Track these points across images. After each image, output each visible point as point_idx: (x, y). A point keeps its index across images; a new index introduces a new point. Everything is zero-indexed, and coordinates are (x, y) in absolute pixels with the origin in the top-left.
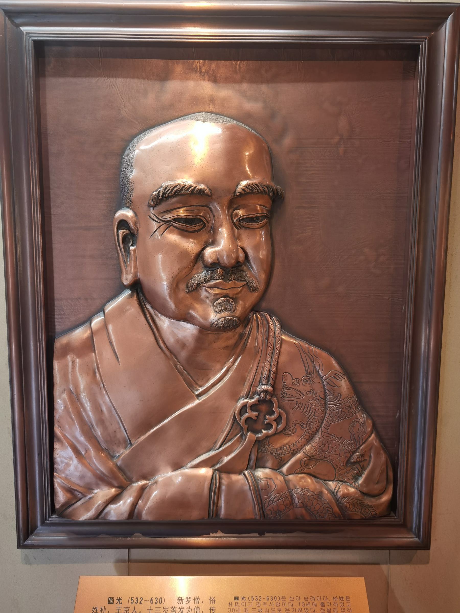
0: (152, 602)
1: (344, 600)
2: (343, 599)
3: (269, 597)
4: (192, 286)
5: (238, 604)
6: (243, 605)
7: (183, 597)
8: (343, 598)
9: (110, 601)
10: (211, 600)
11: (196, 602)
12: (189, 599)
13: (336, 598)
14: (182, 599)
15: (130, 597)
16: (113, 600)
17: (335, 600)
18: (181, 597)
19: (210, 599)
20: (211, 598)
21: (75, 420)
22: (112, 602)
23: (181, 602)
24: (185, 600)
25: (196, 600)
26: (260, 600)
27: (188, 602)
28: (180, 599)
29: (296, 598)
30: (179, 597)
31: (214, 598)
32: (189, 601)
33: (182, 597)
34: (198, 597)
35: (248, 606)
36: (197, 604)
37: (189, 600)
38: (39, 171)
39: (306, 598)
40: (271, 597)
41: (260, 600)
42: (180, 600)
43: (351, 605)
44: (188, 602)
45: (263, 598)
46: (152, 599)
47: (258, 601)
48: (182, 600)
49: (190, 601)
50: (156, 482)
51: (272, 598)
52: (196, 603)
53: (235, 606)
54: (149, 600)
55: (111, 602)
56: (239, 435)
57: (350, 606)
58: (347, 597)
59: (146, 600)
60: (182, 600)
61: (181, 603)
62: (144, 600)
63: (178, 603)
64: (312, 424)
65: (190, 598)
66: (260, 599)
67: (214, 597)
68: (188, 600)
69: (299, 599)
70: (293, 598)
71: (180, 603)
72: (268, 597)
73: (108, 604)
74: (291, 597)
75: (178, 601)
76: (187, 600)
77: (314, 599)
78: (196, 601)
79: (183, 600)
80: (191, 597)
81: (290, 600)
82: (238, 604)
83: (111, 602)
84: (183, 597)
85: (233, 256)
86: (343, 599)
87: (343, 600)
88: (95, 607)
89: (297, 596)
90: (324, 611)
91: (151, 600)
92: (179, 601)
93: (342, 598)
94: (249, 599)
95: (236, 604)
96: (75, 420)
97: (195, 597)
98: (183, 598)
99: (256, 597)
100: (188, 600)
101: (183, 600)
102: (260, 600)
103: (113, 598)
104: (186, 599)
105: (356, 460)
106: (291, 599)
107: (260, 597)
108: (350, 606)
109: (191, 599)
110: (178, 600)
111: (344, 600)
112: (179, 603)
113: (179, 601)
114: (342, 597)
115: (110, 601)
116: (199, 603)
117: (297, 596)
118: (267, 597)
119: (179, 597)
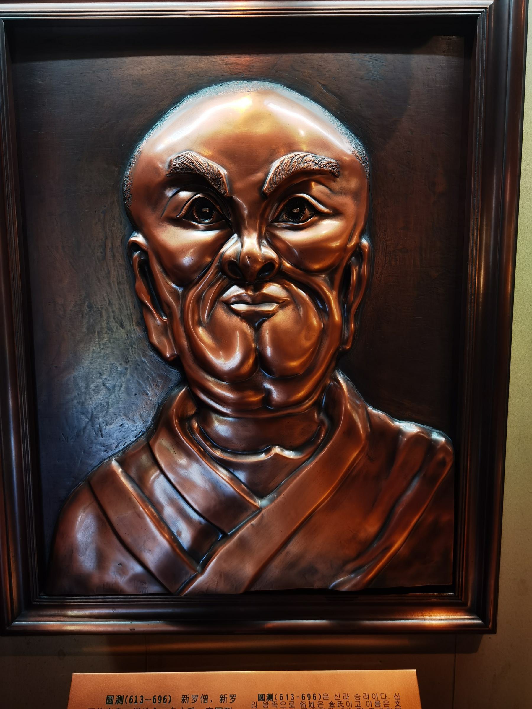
2: (313, 705)
3: (282, 696)
4: (472, 298)
5: (341, 703)
6: (368, 705)
8: (314, 704)
9: (109, 701)
11: (204, 701)
12: (196, 697)
13: (304, 704)
14: (225, 697)
16: (263, 696)
22: (262, 698)
23: (186, 701)
24: (229, 699)
25: (204, 698)
27: (194, 700)
28: (223, 697)
29: (344, 696)
30: (222, 695)
32: (234, 700)
33: (225, 695)
34: (206, 695)
37: (195, 698)
38: (41, 20)
39: (357, 696)
40: (291, 695)
42: (223, 698)
43: (360, 706)
44: (194, 700)
46: (155, 698)
47: (312, 700)
51: (293, 697)
52: (204, 702)
53: (338, 706)
54: (151, 699)
55: (110, 701)
56: (318, 302)
57: (360, 707)
58: (319, 702)
59: (275, 696)
61: (186, 702)
63: (221, 701)
68: (194, 699)
70: (338, 696)
71: (223, 702)
73: (107, 703)
74: (336, 695)
75: (182, 699)
76: (231, 698)
77: (368, 697)
78: (204, 700)
79: (188, 698)
80: (236, 695)
81: (394, 698)
82: (341, 703)
83: (110, 701)
86: (313, 705)
91: (154, 698)
92: (184, 699)
93: (312, 704)
95: (339, 704)
97: (203, 695)
98: (188, 696)
99: (292, 695)
100: (232, 698)
101: (189, 699)
103: (112, 697)
104: (230, 697)
106: (396, 697)
109: (198, 697)
110: (220, 698)
112: (221, 702)
113: (222, 699)
115: (109, 701)
116: (207, 702)
117: (364, 694)
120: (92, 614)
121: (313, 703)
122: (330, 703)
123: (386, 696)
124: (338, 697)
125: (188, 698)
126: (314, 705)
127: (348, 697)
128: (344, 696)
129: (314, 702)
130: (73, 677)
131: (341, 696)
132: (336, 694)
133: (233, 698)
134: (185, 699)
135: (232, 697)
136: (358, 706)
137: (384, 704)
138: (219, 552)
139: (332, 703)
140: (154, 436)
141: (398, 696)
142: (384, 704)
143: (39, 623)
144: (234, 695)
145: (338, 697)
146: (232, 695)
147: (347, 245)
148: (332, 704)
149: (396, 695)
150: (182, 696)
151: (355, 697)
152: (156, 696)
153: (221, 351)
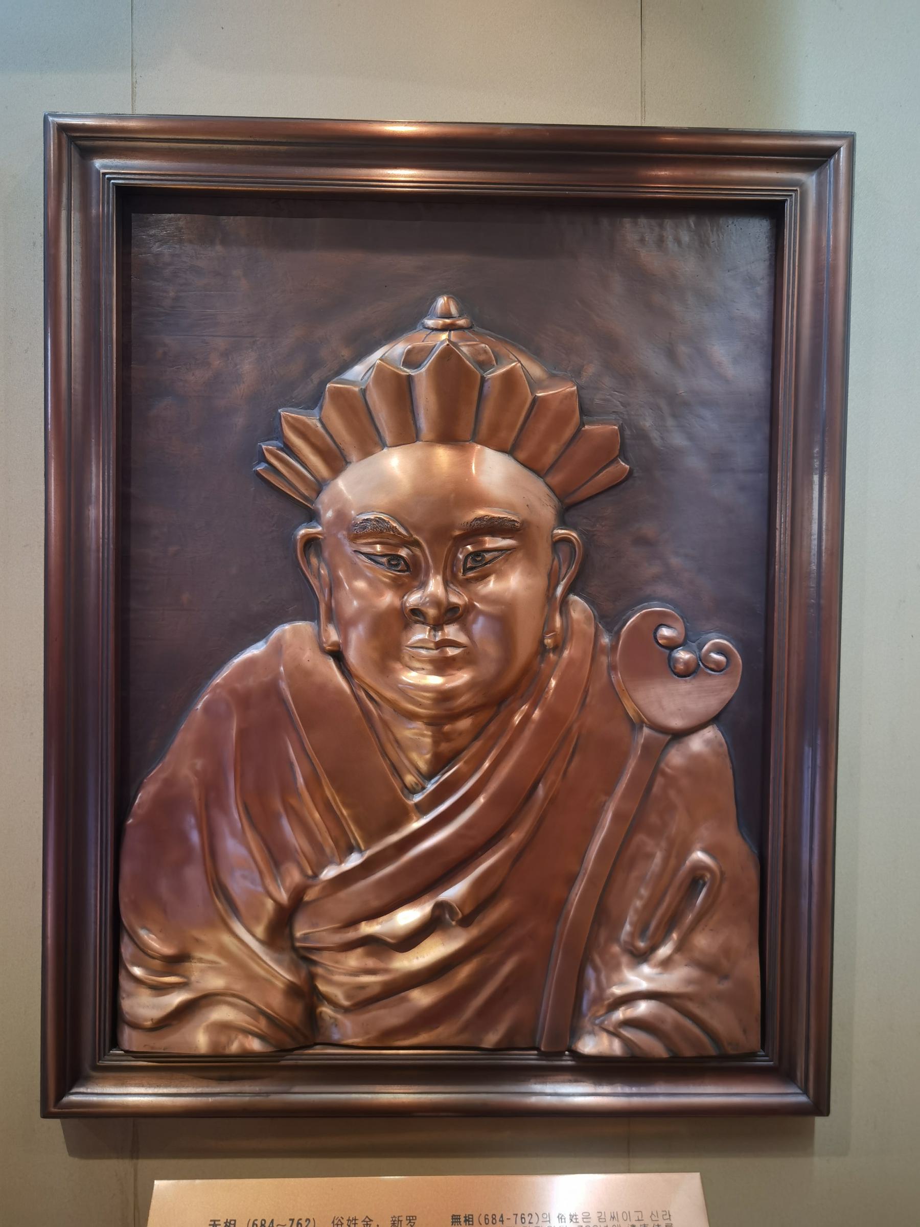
0: (487, 1222)
1: (578, 1222)
2: (576, 1219)
3: (488, 1217)
7: (402, 1216)
8: (577, 1217)
10: (335, 1223)
12: (413, 1219)
14: (399, 1220)
15: (481, 1215)
17: (562, 1222)
18: (397, 1216)
19: (333, 1222)
20: (336, 1218)
21: (558, 601)
26: (531, 1222)
27: (411, 1225)
29: (663, 1215)
30: (394, 1217)
31: (342, 1220)
32: (412, 1224)
33: (399, 1217)
35: (636, 1220)
36: (563, 1223)
41: (530, 1223)
43: (643, 1219)
45: (508, 1219)
48: (400, 1222)
49: (414, 1223)
50: (345, 538)
57: (643, 1220)
59: (479, 1217)
60: (400, 1222)
62: (527, 1215)
64: (550, 638)
65: (414, 1218)
66: (530, 1220)
67: (342, 1217)
68: (410, 1222)
69: (548, 1220)
72: (524, 1215)
74: (652, 1214)
76: (409, 1221)
79: (401, 1221)
80: (416, 1217)
84: (402, 1216)
85: (723, 230)
86: (576, 1219)
87: (578, 1220)
88: (351, 1219)
89: (663, 1211)
90: (656, 1219)
94: (481, 1222)
96: (558, 601)
97: (335, 1217)
98: (400, 1219)
101: (402, 1222)
102: (530, 1223)
104: (407, 1220)
105: (364, 392)
107: (530, 1216)
108: (643, 1220)
110: (391, 1221)
111: (578, 1222)
114: (576, 1216)
117: (663, 1211)
118: (485, 1217)
119: (394, 1217)
120: (622, 1085)
121: (355, 1220)
122: (214, 1221)
123: (670, 1216)
124: (655, 1216)
125: (401, 1221)
126: (357, 1224)
127: (670, 1216)
128: (663, 1215)
129: (357, 1218)
130: (155, 1187)
131: (660, 1214)
132: (652, 1212)
133: (412, 1221)
134: (395, 1222)
135: (410, 1220)
136: (639, 1220)
137: (583, 1218)
138: (153, 980)
139: (367, 1220)
140: (574, 641)
141: (656, 1215)
142: (583, 1218)
143: (546, 1027)
144: (413, 1217)
145: (655, 1216)
146: (409, 1217)
147: (544, 639)
148: (367, 1222)
149: (652, 1214)
150: (392, 1217)
151: (589, 1217)
152: (256, 1220)
153: (92, 160)
